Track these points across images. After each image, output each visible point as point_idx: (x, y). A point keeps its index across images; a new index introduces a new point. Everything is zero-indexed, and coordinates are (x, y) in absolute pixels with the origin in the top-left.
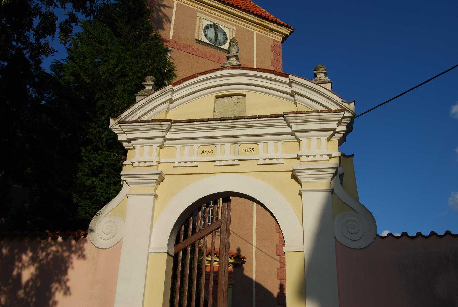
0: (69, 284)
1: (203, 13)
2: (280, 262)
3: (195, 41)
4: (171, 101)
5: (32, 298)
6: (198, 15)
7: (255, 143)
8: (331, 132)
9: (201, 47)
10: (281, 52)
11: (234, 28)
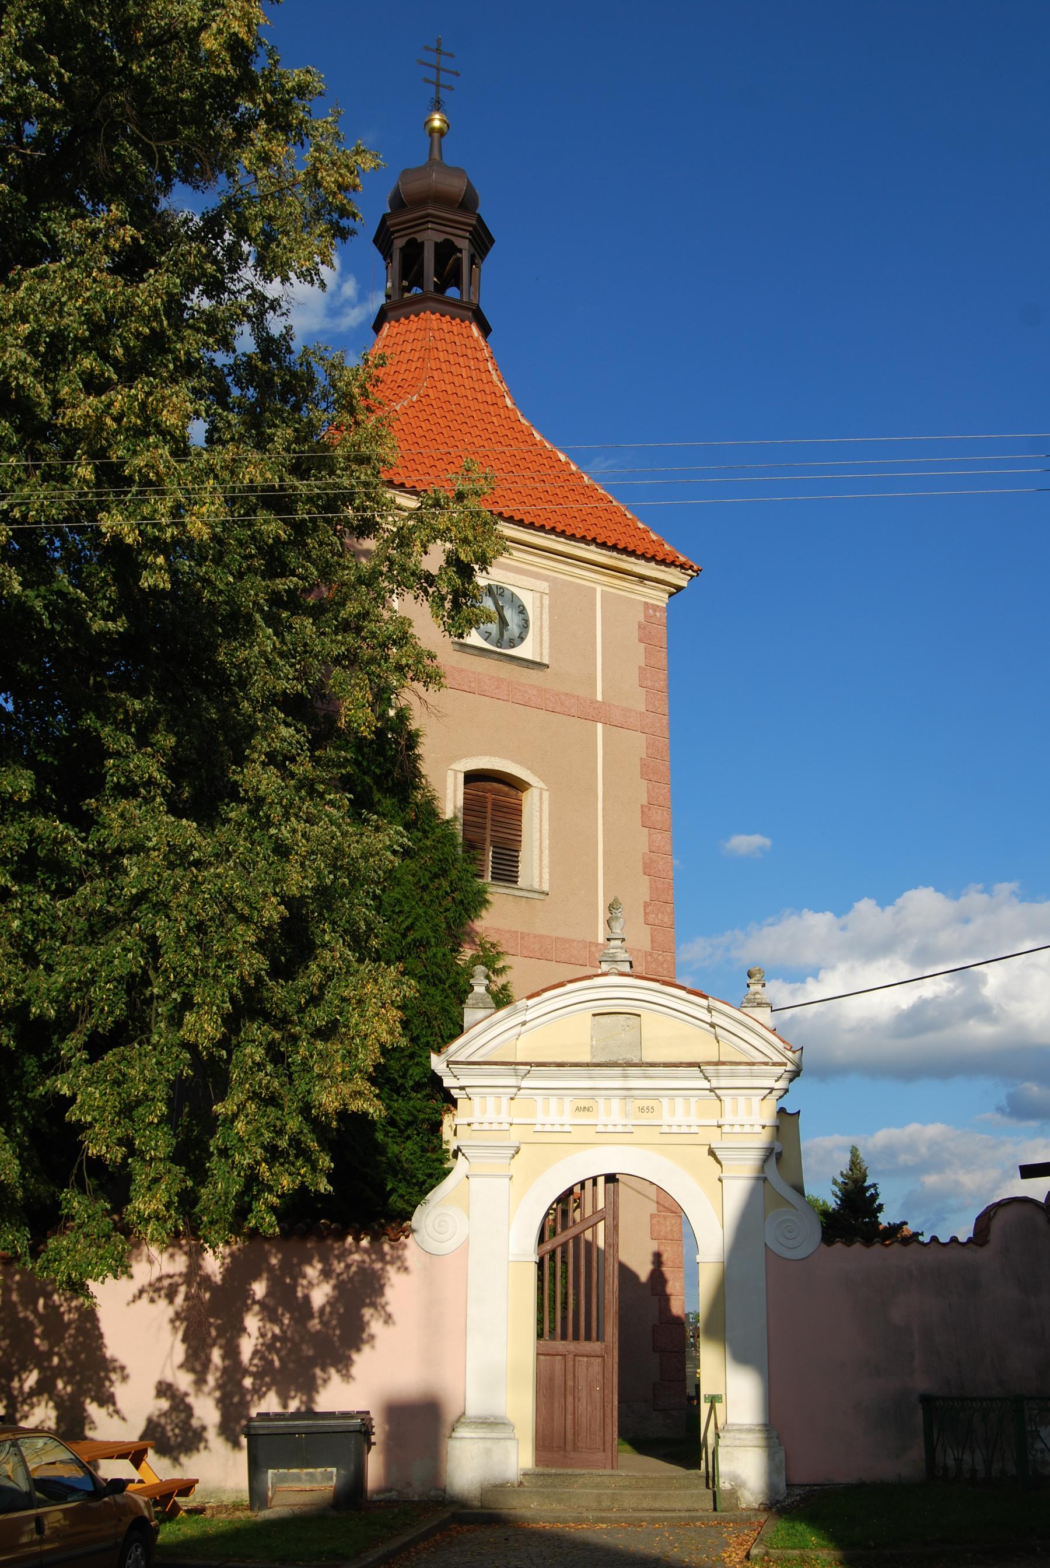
0: (389, 1309)
2: (657, 1203)
4: (524, 1023)
7: (656, 1098)
10: (665, 639)
11: (544, 586)
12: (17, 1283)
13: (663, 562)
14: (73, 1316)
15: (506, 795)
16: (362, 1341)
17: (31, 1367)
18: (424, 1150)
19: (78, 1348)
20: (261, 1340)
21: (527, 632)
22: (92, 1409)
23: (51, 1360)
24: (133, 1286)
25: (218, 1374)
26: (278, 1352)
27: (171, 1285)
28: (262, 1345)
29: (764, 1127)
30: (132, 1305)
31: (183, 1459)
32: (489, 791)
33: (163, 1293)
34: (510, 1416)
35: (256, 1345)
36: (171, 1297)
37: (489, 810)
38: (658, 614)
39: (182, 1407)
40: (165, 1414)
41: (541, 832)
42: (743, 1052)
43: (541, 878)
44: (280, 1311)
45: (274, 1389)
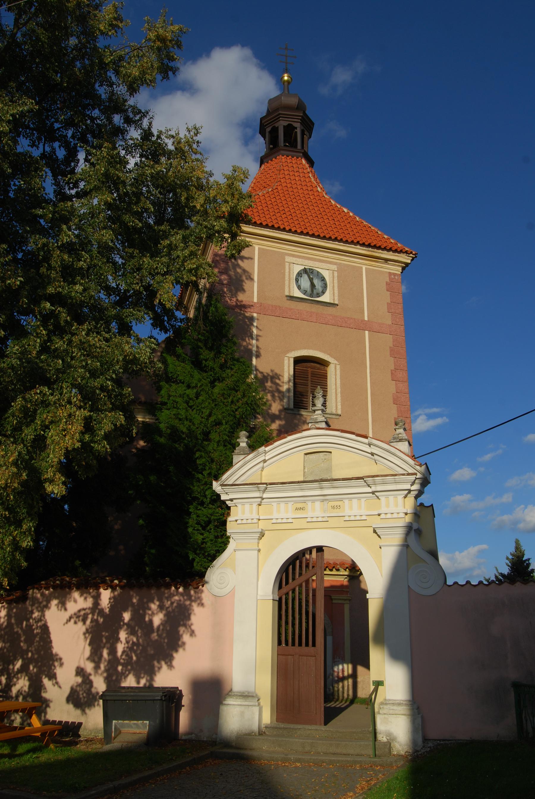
0: (193, 627)
1: (293, 256)
3: (286, 298)
4: (265, 461)
5: (164, 639)
6: (286, 260)
8: (407, 492)
11: (335, 267)
12: (15, 613)
13: (396, 251)
14: (39, 631)
15: (319, 369)
16: (179, 646)
17: (19, 658)
18: (217, 537)
19: (40, 648)
20: (126, 645)
21: (326, 290)
22: (46, 681)
23: (28, 654)
24: (67, 615)
25: (106, 663)
26: (135, 652)
27: (84, 614)
28: (127, 647)
29: (406, 514)
30: (66, 625)
31: (87, 711)
32: (309, 367)
33: (81, 618)
34: (259, 693)
35: (124, 648)
36: (84, 621)
37: (309, 376)
38: (396, 277)
39: (88, 681)
40: (79, 685)
41: (336, 385)
42: (390, 468)
43: (337, 407)
44: (137, 628)
45: (132, 672)
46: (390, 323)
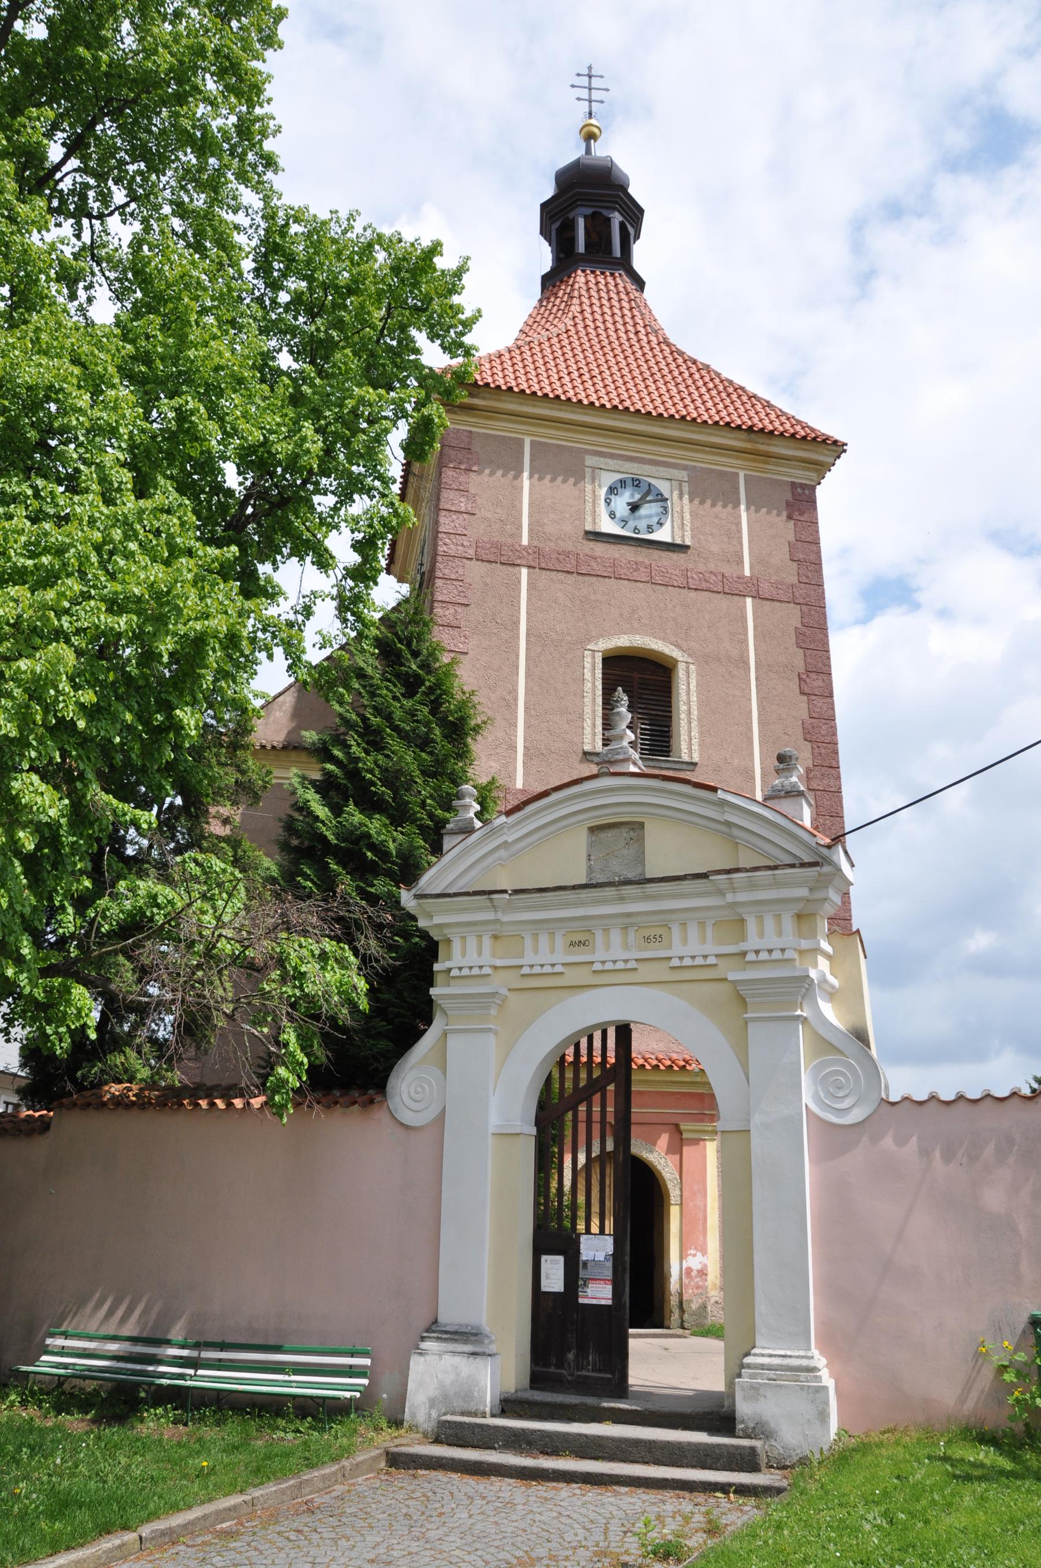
9: (600, 549)
11: (683, 475)
46: (794, 580)
